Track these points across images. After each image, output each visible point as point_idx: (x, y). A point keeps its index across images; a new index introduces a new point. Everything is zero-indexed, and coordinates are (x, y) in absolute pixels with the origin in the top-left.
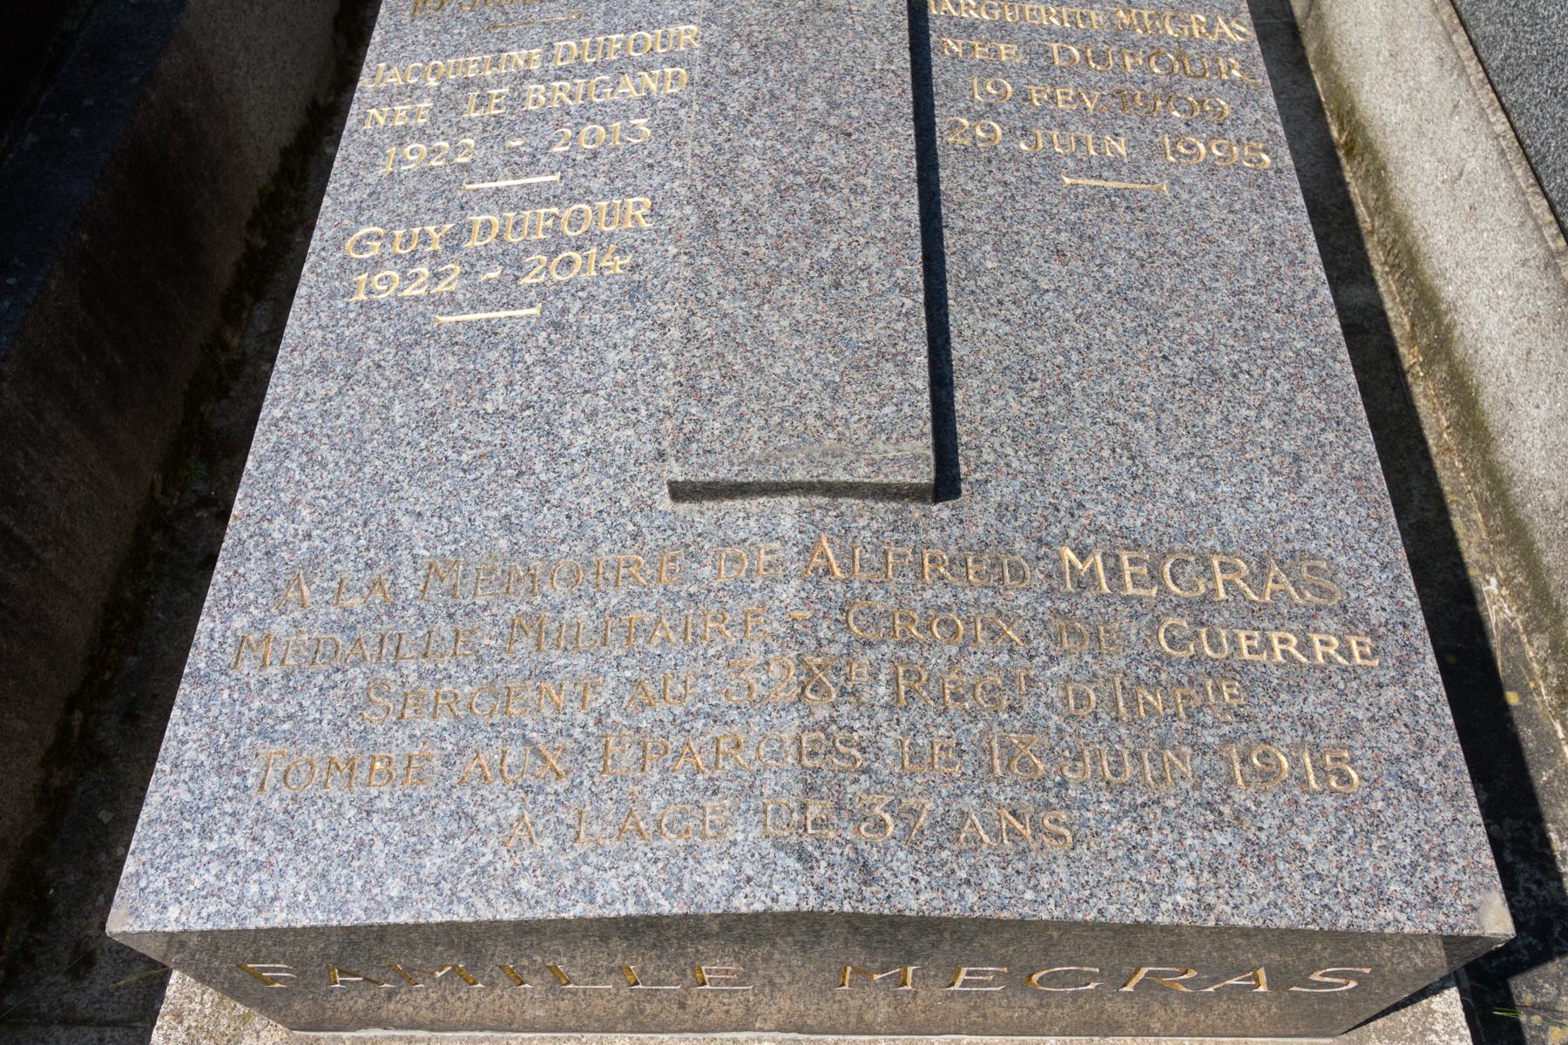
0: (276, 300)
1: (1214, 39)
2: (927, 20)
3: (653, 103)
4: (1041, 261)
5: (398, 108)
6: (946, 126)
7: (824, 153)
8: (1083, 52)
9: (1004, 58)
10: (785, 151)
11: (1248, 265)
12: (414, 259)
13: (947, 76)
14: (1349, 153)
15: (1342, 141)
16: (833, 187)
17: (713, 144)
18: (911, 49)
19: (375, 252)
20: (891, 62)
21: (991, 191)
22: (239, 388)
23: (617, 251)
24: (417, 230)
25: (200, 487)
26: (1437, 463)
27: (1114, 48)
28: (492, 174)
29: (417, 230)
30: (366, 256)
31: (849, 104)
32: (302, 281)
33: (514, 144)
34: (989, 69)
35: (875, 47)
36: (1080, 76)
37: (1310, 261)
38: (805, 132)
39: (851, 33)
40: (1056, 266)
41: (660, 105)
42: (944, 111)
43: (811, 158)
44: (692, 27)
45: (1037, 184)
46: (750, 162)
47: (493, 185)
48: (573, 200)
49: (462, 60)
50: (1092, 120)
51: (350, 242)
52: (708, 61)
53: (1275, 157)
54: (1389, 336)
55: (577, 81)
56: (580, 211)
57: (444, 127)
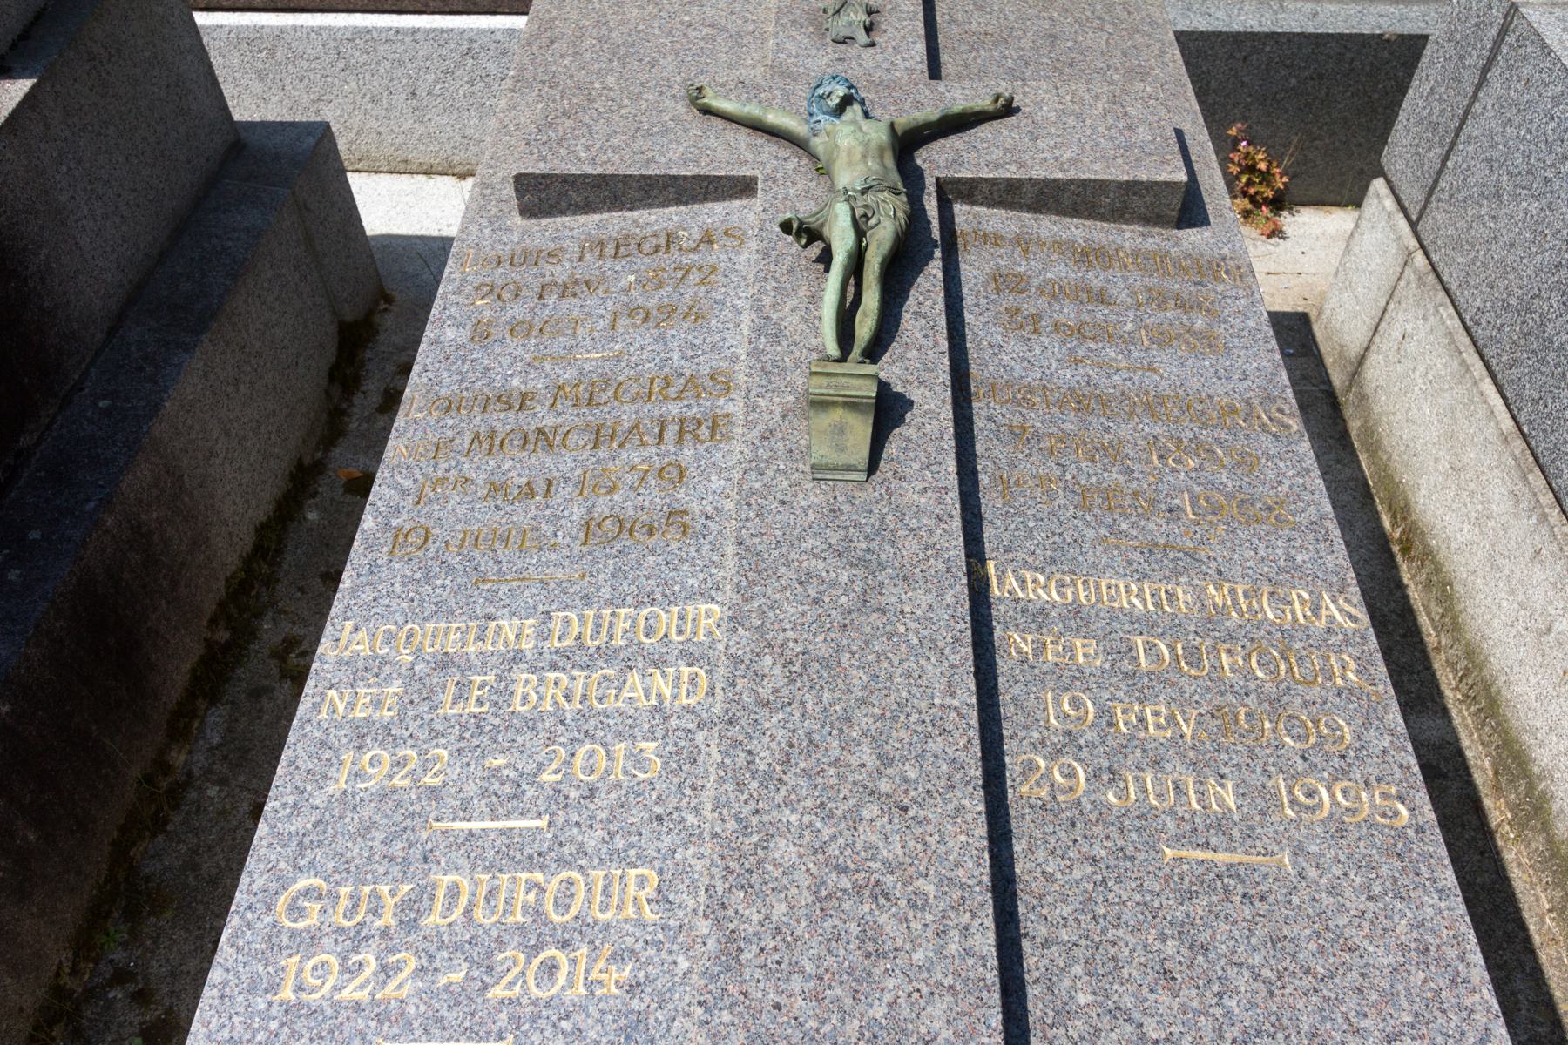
0: (233, 703)
1: (1322, 624)
2: (989, 607)
3: (666, 718)
4: (1145, 990)
5: (362, 691)
6: (1018, 769)
7: (873, 838)
8: (1173, 650)
9: (1081, 659)
10: (827, 832)
11: (1400, 987)
12: (359, 938)
13: (1016, 690)
14: (1405, 550)
15: (1397, 535)
16: (887, 896)
17: (739, 820)
18: (976, 674)
19: (312, 920)
20: (953, 695)
21: (1077, 874)
22: (178, 819)
23: (613, 956)
24: (367, 889)
25: (119, 955)
26: (1543, 958)
27: (1209, 642)
28: (465, 810)
29: (367, 889)
30: (300, 925)
31: (904, 759)
32: (218, 958)
33: (496, 763)
34: (1069, 678)
35: (933, 670)
36: (1172, 685)
37: (1476, 980)
38: (852, 802)
39: (904, 647)
40: (1165, 999)
41: (674, 722)
42: (1015, 743)
43: (859, 846)
44: (714, 607)
45: (1132, 859)
46: (783, 849)
47: (466, 825)
48: (562, 863)
49: (443, 625)
50: (1191, 754)
51: (282, 901)
52: (733, 684)
53: (1415, 810)
54: (1469, 783)
55: (575, 673)
56: (570, 882)
57: (414, 726)
